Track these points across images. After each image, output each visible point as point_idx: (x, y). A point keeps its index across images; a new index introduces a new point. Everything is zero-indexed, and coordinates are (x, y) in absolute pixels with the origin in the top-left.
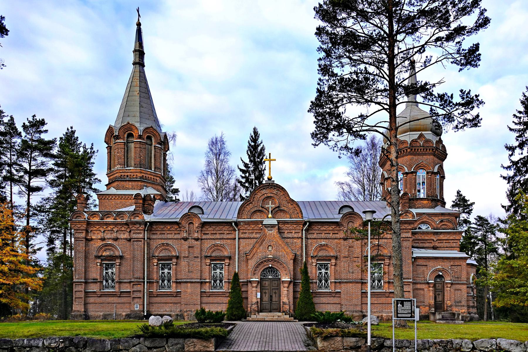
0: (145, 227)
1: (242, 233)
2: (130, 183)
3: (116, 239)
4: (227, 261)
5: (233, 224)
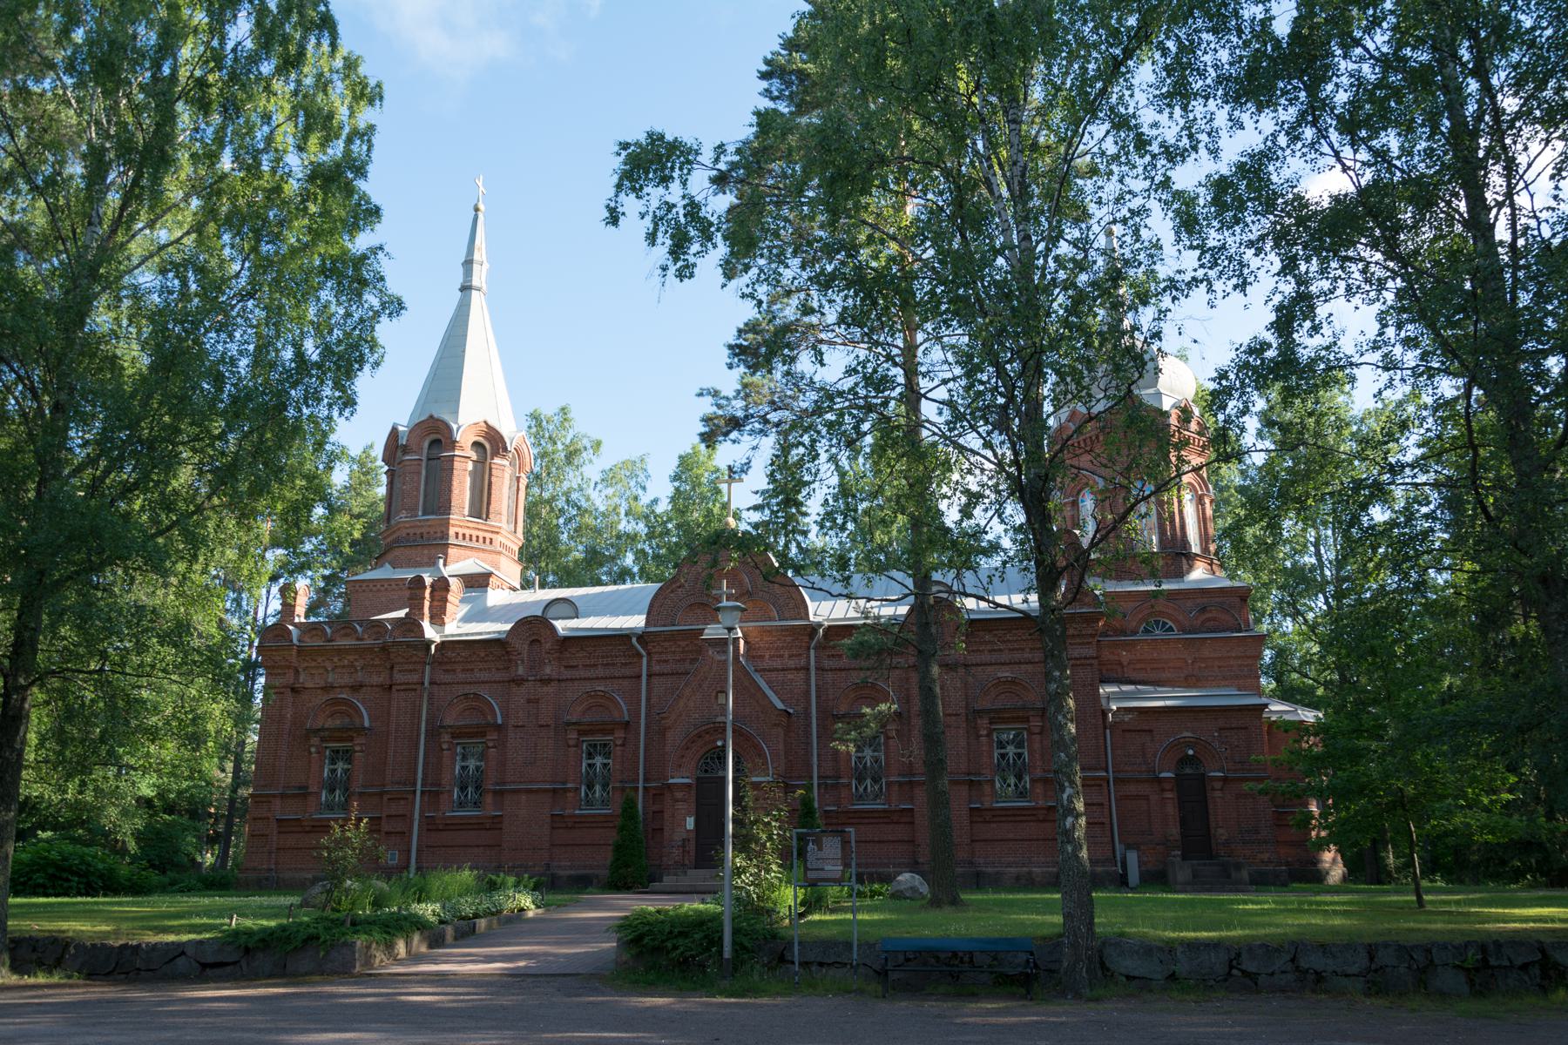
1: (659, 662)
2: (426, 552)
3: (356, 688)
4: (620, 734)
5: (634, 640)
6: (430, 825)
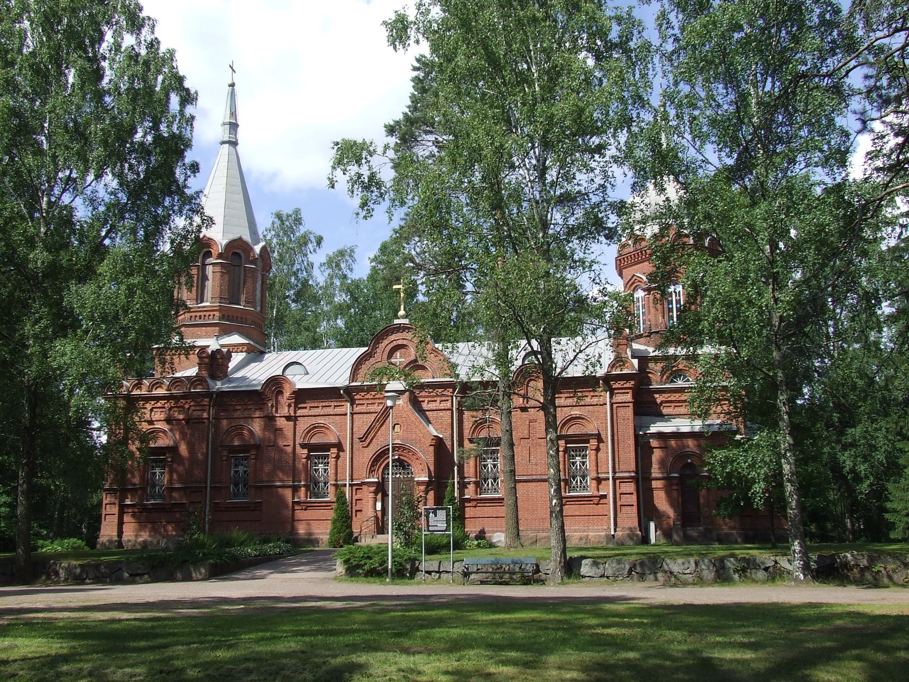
0: (211, 400)
6: (216, 508)
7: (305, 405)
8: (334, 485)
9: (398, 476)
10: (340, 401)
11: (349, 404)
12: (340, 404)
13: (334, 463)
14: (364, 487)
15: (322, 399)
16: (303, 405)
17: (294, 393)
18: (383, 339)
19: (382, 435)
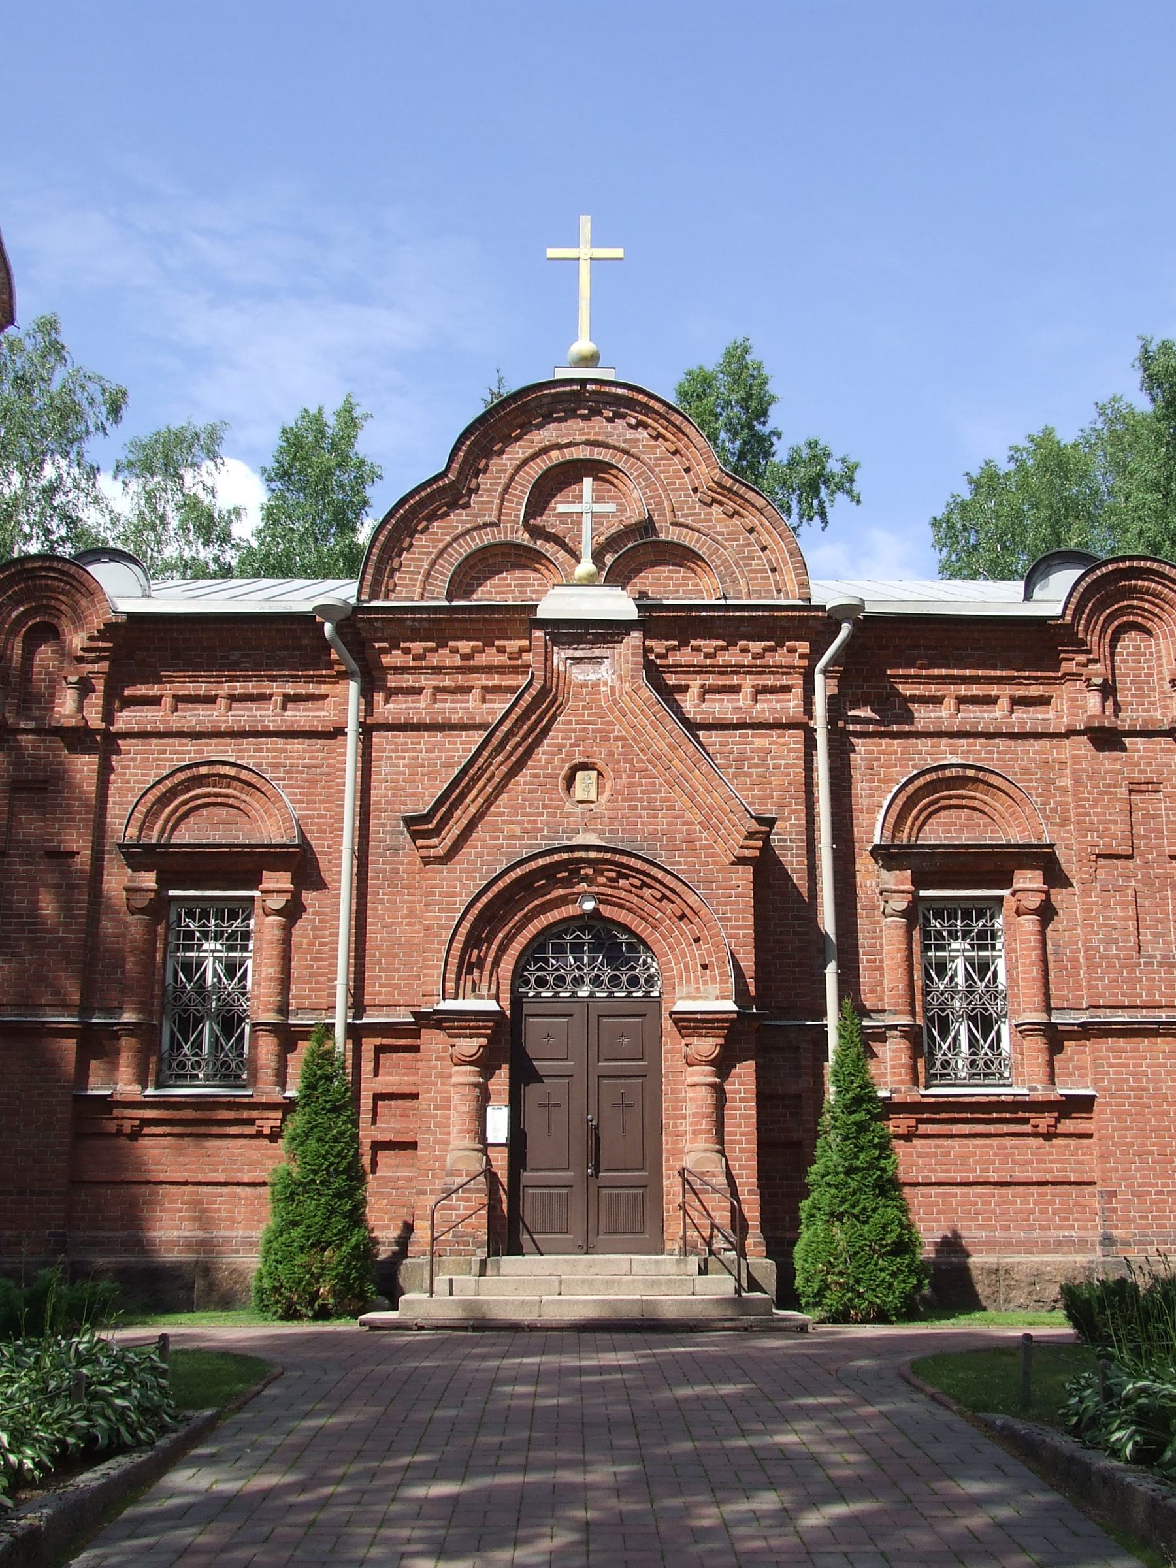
7: (153, 690)
8: (274, 1029)
9: (584, 992)
10: (310, 680)
11: (353, 687)
12: (312, 689)
13: (277, 933)
14: (432, 1040)
15: (234, 666)
16: (142, 690)
17: (110, 630)
18: (508, 440)
19: (515, 809)
